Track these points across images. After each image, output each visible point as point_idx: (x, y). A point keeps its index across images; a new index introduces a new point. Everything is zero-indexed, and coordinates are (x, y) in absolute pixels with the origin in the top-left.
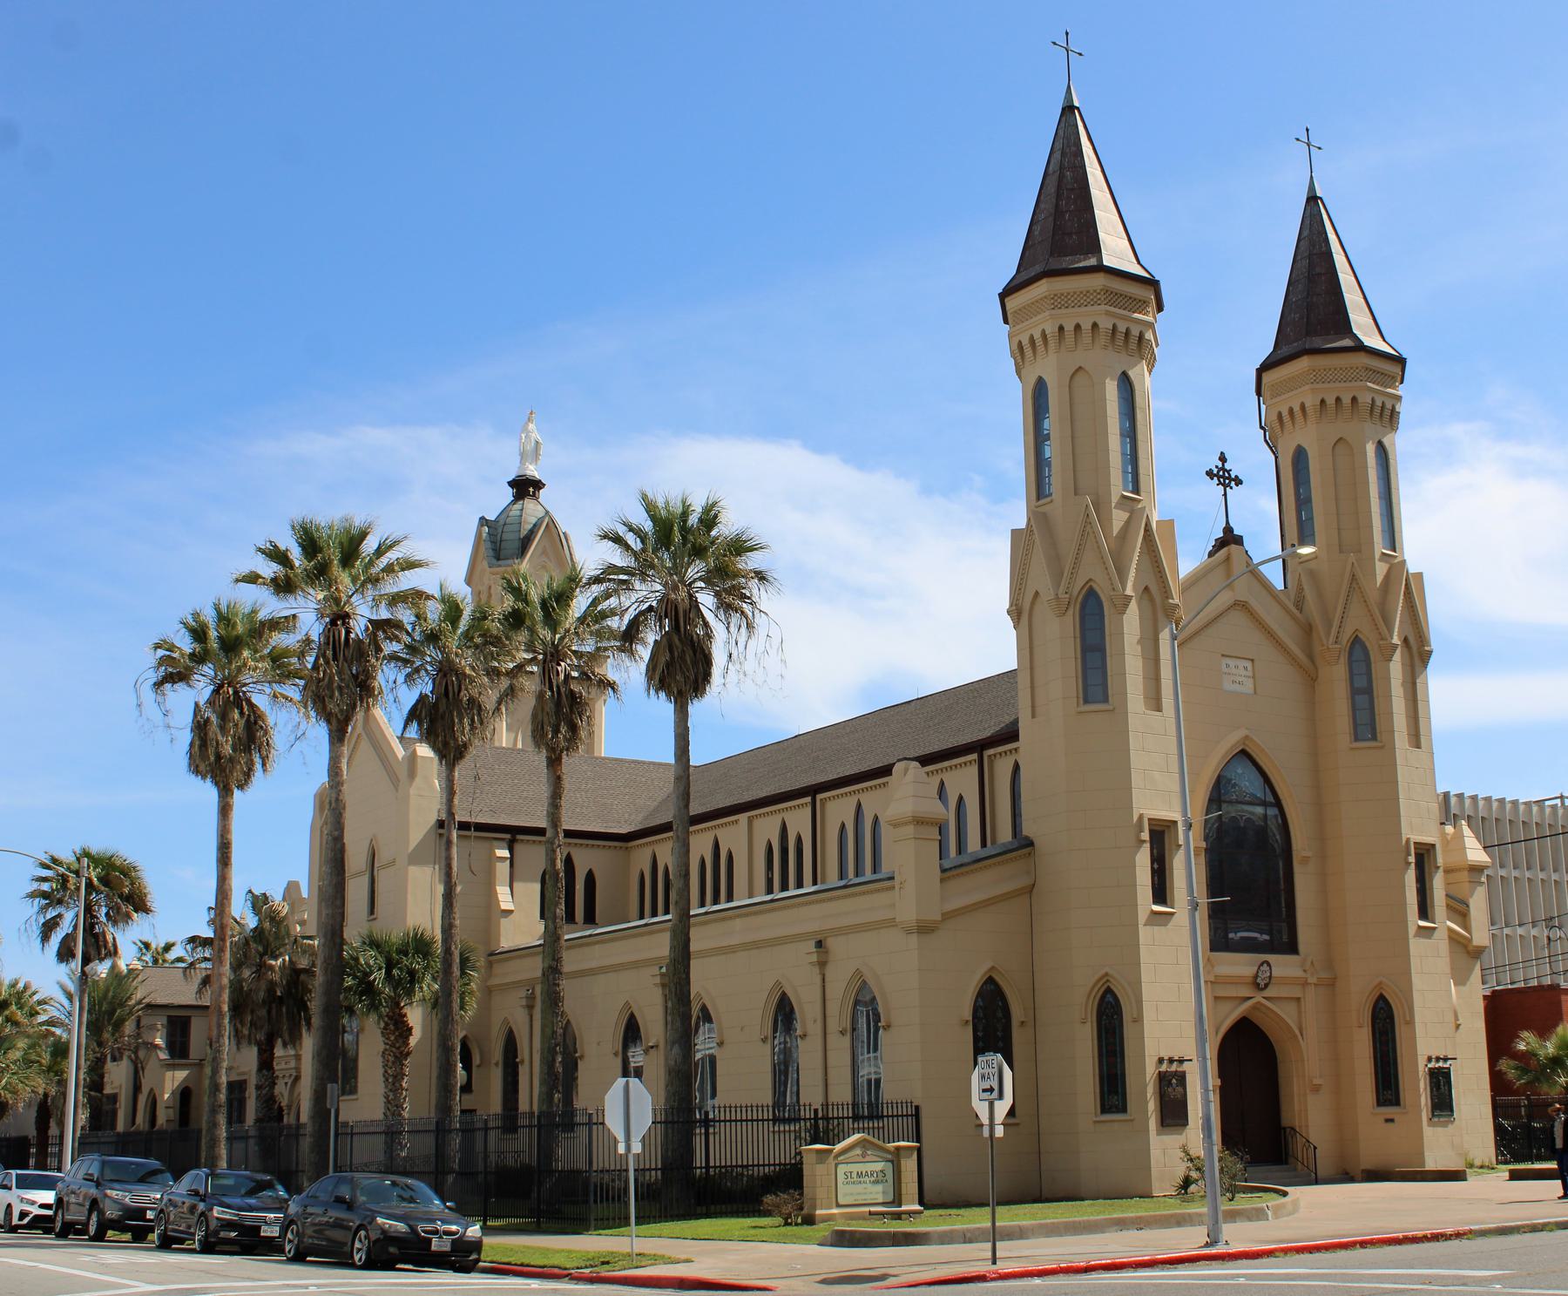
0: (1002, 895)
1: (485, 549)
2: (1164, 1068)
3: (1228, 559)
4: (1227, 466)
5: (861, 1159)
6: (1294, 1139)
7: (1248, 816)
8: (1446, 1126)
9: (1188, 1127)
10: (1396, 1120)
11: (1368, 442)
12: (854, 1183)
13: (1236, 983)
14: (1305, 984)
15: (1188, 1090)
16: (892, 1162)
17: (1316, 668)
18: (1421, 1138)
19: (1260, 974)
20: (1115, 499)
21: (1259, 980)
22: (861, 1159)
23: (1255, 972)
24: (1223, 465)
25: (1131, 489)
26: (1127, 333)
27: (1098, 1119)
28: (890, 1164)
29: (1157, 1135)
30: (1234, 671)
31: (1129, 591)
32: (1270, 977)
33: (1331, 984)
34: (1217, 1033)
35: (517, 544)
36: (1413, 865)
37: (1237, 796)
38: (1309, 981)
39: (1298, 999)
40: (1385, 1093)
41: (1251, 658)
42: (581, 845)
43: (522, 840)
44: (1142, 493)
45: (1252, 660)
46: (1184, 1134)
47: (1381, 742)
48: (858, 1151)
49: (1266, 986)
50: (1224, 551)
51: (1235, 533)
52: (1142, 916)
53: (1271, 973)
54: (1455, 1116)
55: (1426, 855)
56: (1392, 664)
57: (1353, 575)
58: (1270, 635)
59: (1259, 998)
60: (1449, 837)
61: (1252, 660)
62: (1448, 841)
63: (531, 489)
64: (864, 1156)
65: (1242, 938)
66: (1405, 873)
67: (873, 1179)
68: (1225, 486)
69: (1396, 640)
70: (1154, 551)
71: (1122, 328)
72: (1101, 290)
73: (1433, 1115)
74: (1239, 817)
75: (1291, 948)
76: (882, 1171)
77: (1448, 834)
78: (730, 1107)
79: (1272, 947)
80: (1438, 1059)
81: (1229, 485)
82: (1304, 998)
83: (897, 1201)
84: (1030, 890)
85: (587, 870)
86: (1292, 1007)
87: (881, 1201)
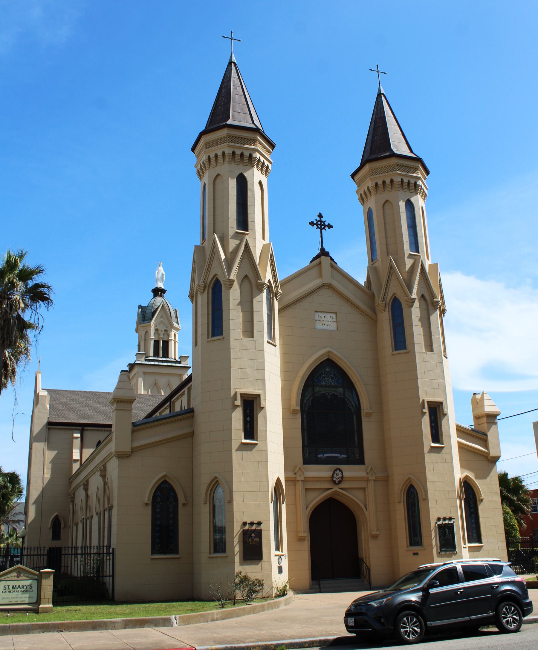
0: (172, 438)
1: (141, 319)
2: (247, 527)
3: (320, 263)
4: (323, 219)
5: (16, 578)
6: (362, 564)
7: (333, 393)
9: (262, 560)
10: (419, 553)
12: (10, 592)
13: (321, 481)
15: (263, 540)
16: (37, 580)
17: (376, 315)
19: (335, 476)
20: (231, 234)
21: (334, 479)
22: (16, 578)
23: (331, 474)
24: (320, 219)
28: (36, 582)
29: (240, 565)
30: (323, 319)
31: (233, 276)
32: (342, 477)
33: (386, 480)
34: (307, 509)
35: (151, 314)
36: (427, 414)
37: (325, 382)
38: (370, 478)
39: (364, 489)
41: (336, 312)
42: (96, 430)
43: (87, 430)
44: (249, 230)
45: (336, 313)
46: (260, 564)
47: (408, 350)
48: (15, 574)
49: (340, 482)
50: (317, 261)
51: (326, 251)
53: (342, 475)
54: (457, 550)
55: (438, 408)
56: (413, 309)
57: (391, 266)
58: (347, 299)
60: (478, 401)
61: (336, 313)
62: (477, 402)
63: (160, 293)
64: (18, 576)
65: (327, 457)
66: (422, 418)
67: (23, 590)
68: (321, 229)
69: (414, 295)
71: (238, 152)
72: (227, 136)
73: (441, 551)
74: (327, 394)
75: (361, 461)
76: (30, 585)
77: (477, 399)
78: (31, 548)
79: (348, 462)
80: (445, 519)
81: (324, 228)
82: (368, 487)
83: (38, 602)
84: (192, 435)
85: (98, 440)
86: (360, 494)
87: (27, 602)
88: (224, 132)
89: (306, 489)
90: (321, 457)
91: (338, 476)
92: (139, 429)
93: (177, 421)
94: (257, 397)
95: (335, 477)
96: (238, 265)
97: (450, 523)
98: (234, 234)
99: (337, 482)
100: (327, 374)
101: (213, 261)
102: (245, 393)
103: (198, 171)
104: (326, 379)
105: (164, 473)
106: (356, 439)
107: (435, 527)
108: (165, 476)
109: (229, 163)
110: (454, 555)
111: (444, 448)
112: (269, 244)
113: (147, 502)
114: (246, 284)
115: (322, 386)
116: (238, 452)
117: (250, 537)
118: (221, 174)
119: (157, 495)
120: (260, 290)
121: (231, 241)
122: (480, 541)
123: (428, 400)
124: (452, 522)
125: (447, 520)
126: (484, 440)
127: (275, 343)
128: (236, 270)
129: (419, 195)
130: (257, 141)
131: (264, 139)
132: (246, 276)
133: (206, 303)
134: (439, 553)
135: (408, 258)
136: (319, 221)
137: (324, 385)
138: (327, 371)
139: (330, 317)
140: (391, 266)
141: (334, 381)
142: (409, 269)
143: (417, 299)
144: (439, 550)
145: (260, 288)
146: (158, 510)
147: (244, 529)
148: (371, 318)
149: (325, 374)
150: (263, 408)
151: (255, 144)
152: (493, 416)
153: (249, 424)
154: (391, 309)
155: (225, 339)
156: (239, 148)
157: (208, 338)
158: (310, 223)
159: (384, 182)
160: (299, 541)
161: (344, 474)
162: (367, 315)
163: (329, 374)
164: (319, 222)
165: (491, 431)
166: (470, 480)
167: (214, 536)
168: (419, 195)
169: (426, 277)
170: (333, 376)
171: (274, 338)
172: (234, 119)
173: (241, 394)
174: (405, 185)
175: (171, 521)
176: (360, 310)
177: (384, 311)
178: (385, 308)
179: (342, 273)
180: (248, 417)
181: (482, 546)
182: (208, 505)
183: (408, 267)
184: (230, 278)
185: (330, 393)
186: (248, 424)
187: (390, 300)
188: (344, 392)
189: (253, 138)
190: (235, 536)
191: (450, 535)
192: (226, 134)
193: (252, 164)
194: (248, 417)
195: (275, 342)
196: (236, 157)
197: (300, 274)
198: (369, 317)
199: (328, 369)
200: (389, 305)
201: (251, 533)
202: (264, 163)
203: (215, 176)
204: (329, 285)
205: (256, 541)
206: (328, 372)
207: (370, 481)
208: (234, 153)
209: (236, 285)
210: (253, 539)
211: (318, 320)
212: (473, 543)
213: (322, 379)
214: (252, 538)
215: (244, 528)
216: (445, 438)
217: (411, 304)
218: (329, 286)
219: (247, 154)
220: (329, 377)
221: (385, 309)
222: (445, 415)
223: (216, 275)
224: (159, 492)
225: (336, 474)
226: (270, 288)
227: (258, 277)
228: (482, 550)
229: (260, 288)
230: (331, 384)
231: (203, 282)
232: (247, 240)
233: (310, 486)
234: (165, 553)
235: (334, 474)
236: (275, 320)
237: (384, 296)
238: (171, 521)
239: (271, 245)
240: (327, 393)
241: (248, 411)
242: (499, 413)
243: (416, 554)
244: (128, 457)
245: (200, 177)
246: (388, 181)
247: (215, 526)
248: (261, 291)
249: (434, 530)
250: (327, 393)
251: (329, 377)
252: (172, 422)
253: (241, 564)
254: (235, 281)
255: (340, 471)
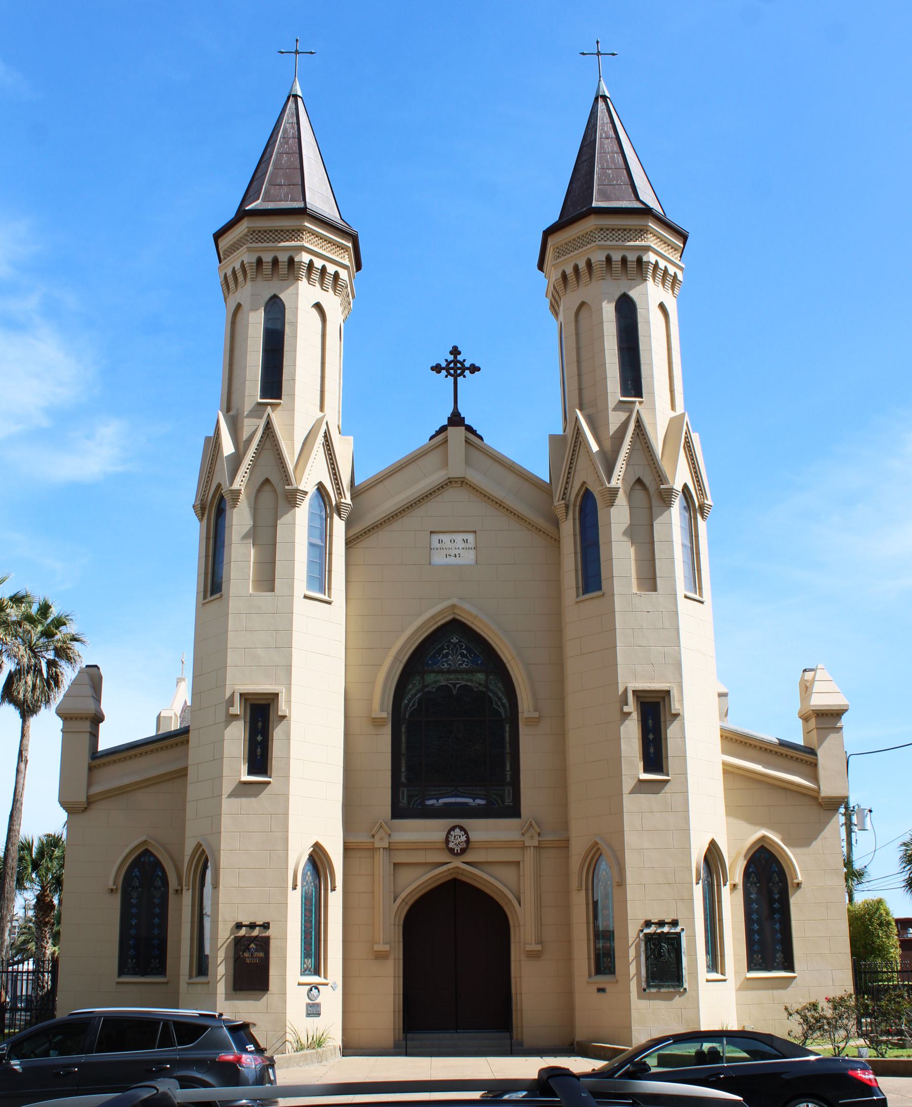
2: (243, 932)
3: (445, 441)
4: (460, 358)
7: (464, 683)
8: (671, 999)
9: (269, 992)
10: (608, 990)
11: (604, 301)
14: (524, 848)
18: (629, 1009)
19: (451, 839)
21: (451, 845)
25: (633, 393)
26: (624, 260)
27: (192, 981)
30: (449, 545)
32: (468, 841)
36: (635, 716)
37: (448, 664)
39: (518, 863)
40: (306, 960)
45: (475, 532)
49: (463, 851)
50: (441, 437)
52: (628, 784)
53: (468, 837)
54: (686, 985)
55: (661, 704)
58: (499, 504)
59: (457, 863)
61: (475, 532)
65: (445, 804)
66: (622, 724)
70: (276, 445)
71: (616, 257)
72: (248, 232)
73: (649, 986)
75: (514, 812)
80: (661, 924)
82: (524, 861)
86: (508, 874)
88: (591, 223)
89: (395, 864)
90: (433, 805)
91: (459, 840)
92: (104, 764)
93: (169, 747)
94: (274, 697)
95: (453, 842)
96: (251, 463)
97: (672, 931)
98: (253, 407)
99: (457, 850)
100: (452, 648)
101: (579, 458)
102: (250, 692)
103: (551, 304)
104: (450, 657)
105: (144, 838)
106: (508, 768)
107: (638, 939)
108: (145, 842)
109: (253, 280)
110: (678, 996)
111: (670, 783)
112: (683, 415)
113: (177, 888)
114: (639, 494)
115: (441, 672)
116: (233, 799)
117: (247, 950)
118: (589, 303)
119: (133, 875)
120: (291, 504)
121: (247, 422)
122: (790, 967)
123: (635, 687)
124: (678, 930)
125: (666, 925)
126: (811, 763)
127: (702, 597)
128: (246, 473)
129: (650, 280)
130: (647, 231)
131: (659, 223)
132: (267, 481)
133: (572, 533)
134: (644, 990)
135: (615, 409)
136: (451, 362)
137: (445, 670)
138: (452, 643)
139: (462, 540)
140: (578, 429)
141: (467, 662)
142: (616, 432)
143: (621, 492)
144: (644, 985)
145: (291, 499)
146: (134, 901)
147: (236, 935)
148: (548, 535)
149: (448, 649)
150: (284, 717)
151: (645, 238)
152: (832, 714)
153: (260, 748)
154: (580, 515)
155: (223, 598)
156: (615, 249)
157: (578, 596)
158: (433, 369)
159: (576, 269)
160: (376, 959)
161: (470, 837)
162: (540, 530)
163: (457, 648)
164: (453, 364)
165: (826, 744)
166: (771, 845)
167: (595, 943)
168: (650, 280)
169: (646, 443)
170: (465, 652)
171: (700, 589)
172: (605, 196)
173: (241, 695)
174: (617, 266)
175: (156, 919)
176: (526, 521)
177: (566, 518)
178: (566, 513)
179: (491, 455)
180: (260, 735)
181: (795, 978)
182: (583, 893)
183: (613, 427)
184: (233, 487)
185: (458, 683)
186: (258, 748)
187: (577, 495)
188: (487, 680)
189: (298, 228)
190: (220, 948)
191: (672, 955)
192: (246, 230)
193: (296, 275)
194: (260, 735)
195: (701, 595)
196: (629, 266)
197: (403, 466)
198: (544, 533)
199: (455, 639)
200: (575, 506)
201: (249, 942)
202: (666, 269)
203: (577, 305)
204: (462, 480)
205: (257, 957)
206: (455, 644)
207: (529, 849)
208: (609, 259)
209: (621, 499)
210: (252, 954)
211: (437, 549)
212: (773, 971)
213: (441, 659)
214: (250, 951)
215: (237, 933)
216: (672, 763)
217: (611, 500)
218: (463, 482)
219: (283, 258)
220: (456, 654)
221: (566, 516)
222: (677, 715)
223: (584, 483)
224: (136, 870)
225: (455, 837)
226: (325, 497)
227: (660, 477)
228: (793, 984)
229: (291, 499)
230: (461, 667)
231: (561, 498)
232: (269, 414)
233: (402, 858)
234: (143, 974)
235: (450, 836)
236: (701, 555)
237: (566, 488)
238: (156, 919)
239: (687, 418)
240: (449, 683)
241: (650, 722)
242: (845, 708)
243: (601, 990)
244: (83, 811)
245: (556, 313)
246: (582, 265)
247: (596, 927)
248: (668, 504)
249: (633, 946)
250: (451, 684)
251: (458, 654)
252: (162, 748)
253: (228, 998)
254: (620, 490)
255: (461, 831)
